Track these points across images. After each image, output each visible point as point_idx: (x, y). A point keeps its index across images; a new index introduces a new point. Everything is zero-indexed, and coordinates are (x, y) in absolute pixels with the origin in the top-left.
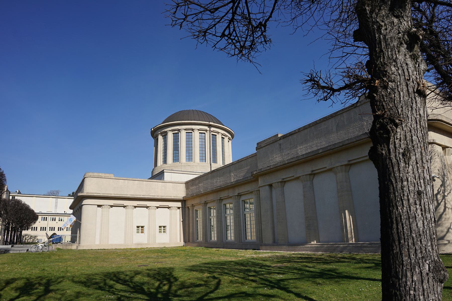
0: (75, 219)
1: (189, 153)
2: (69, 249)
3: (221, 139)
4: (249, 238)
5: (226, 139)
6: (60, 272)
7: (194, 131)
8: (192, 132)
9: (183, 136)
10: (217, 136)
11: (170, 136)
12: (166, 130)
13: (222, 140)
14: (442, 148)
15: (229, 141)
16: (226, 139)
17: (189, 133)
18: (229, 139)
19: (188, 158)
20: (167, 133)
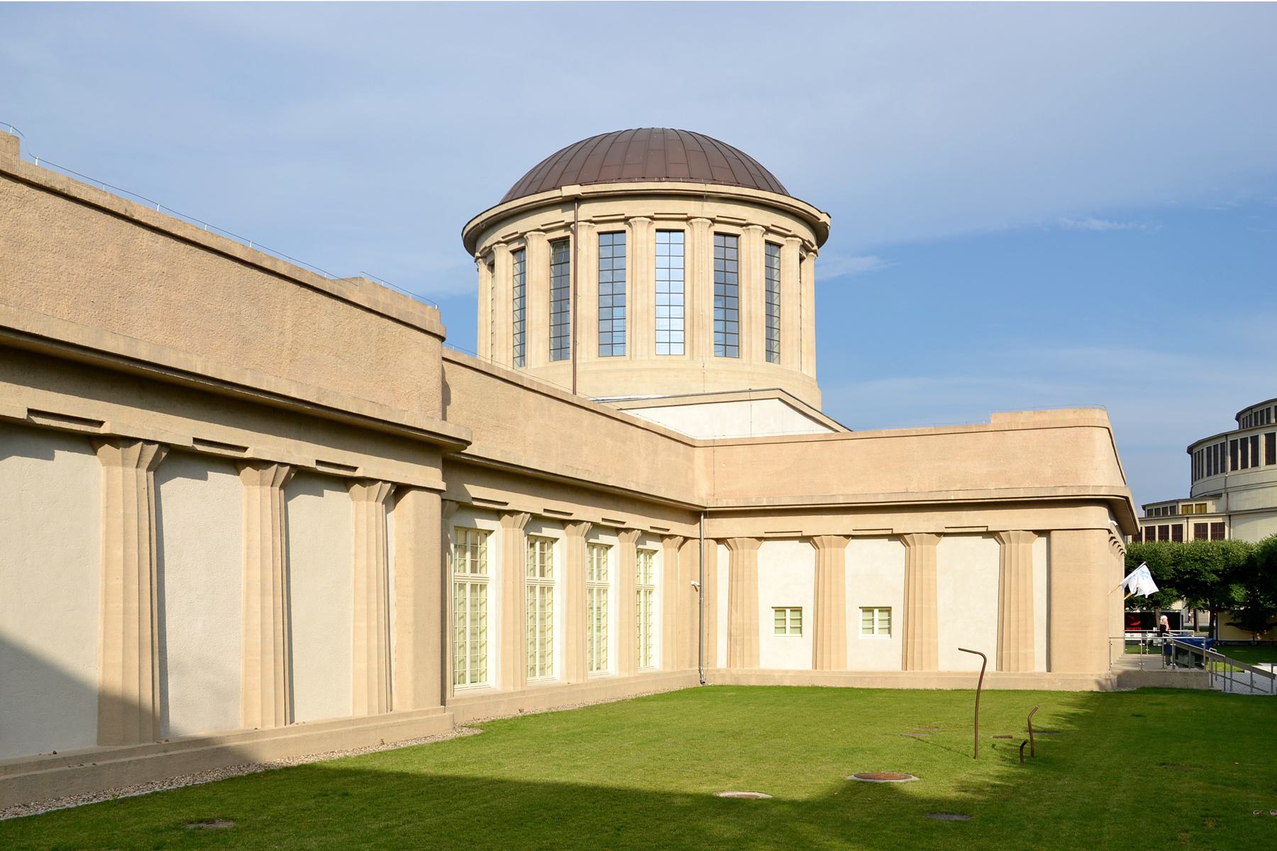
0: (1104, 673)
1: (612, 332)
2: (408, 773)
3: (761, 248)
4: (721, 662)
5: (791, 251)
6: (263, 787)
7: (630, 225)
8: (624, 232)
9: (587, 244)
10: (744, 239)
11: (539, 250)
12: (487, 243)
13: (769, 256)
14: (443, 500)
15: (802, 259)
16: (791, 251)
17: (612, 237)
18: (805, 247)
19: (721, 315)
20: (526, 241)
